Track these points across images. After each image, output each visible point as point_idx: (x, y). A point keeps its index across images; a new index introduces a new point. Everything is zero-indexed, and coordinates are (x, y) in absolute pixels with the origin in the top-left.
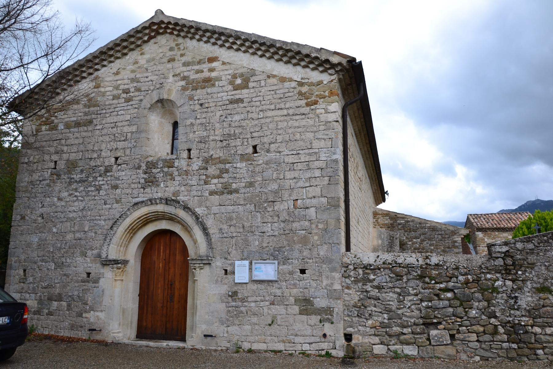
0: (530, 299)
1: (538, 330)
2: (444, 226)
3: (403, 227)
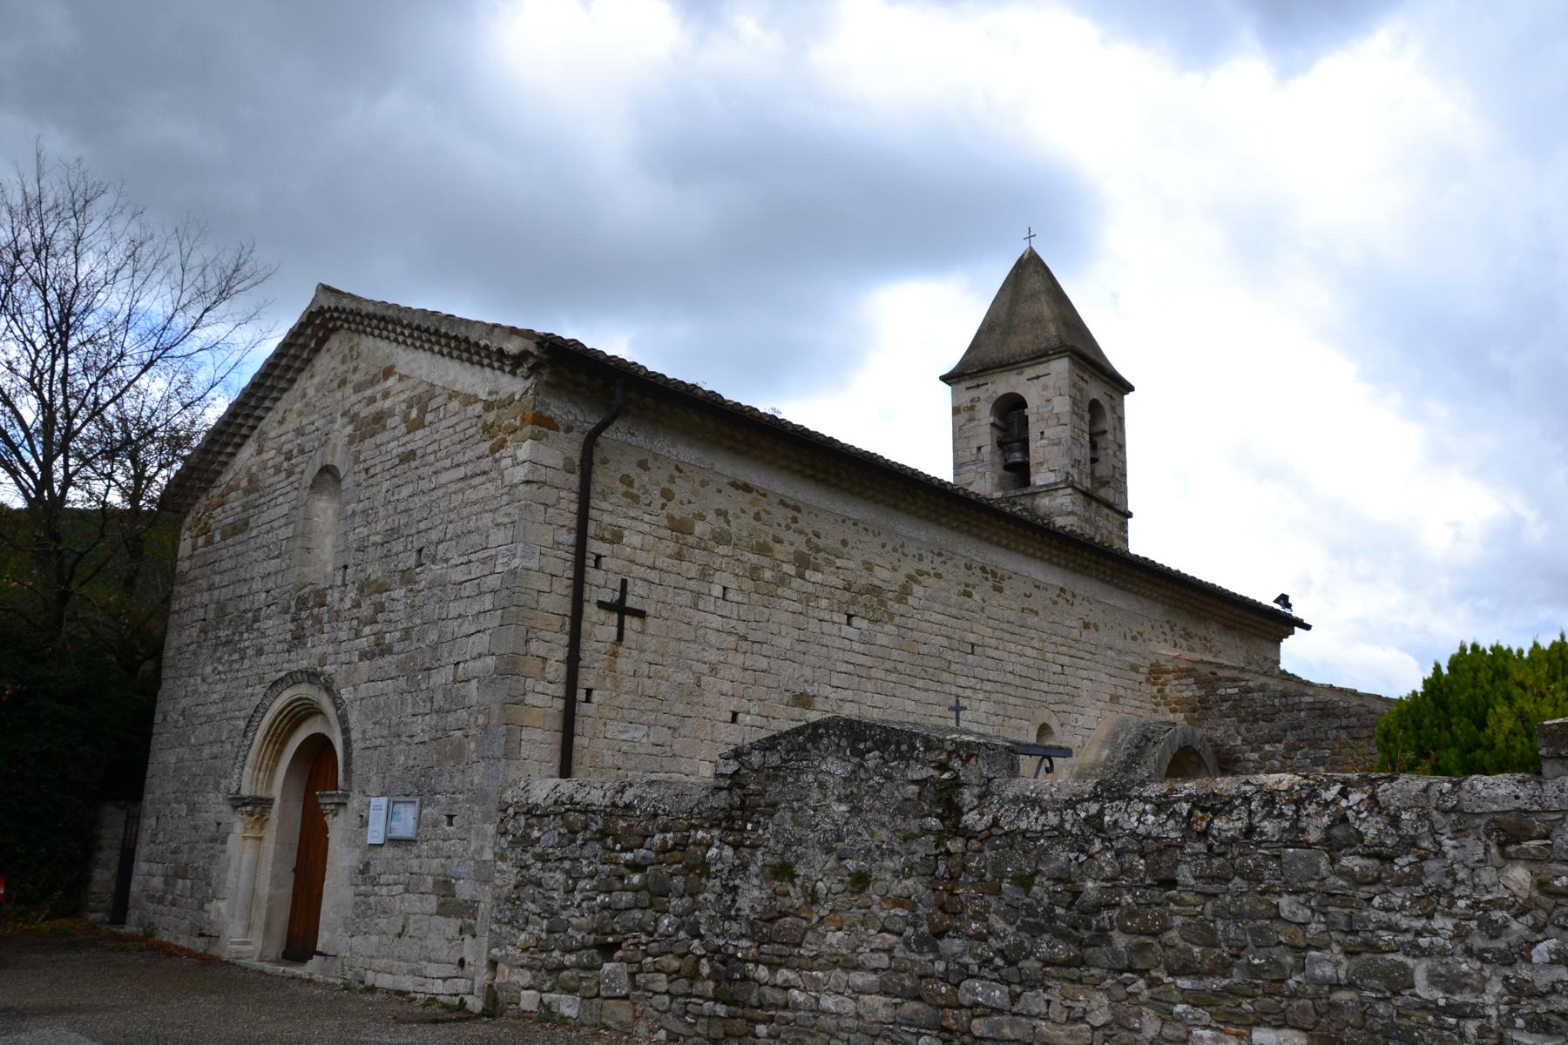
0: (756, 893)
1: (763, 973)
3: (1234, 707)
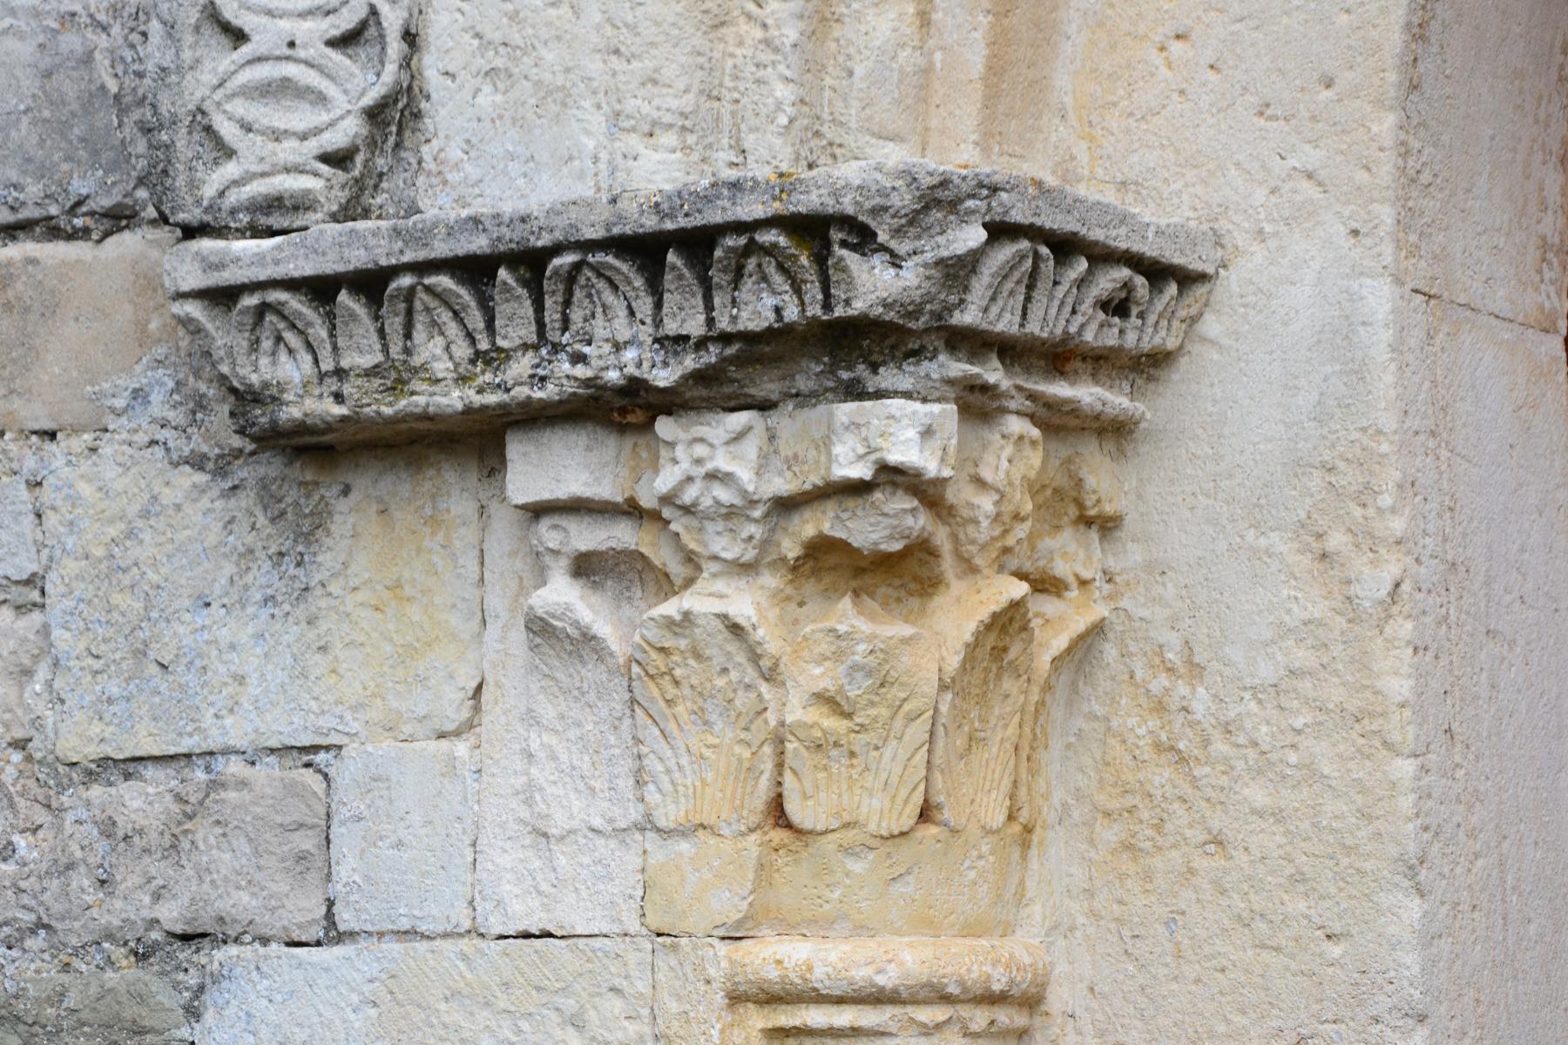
2: (803, 383)
